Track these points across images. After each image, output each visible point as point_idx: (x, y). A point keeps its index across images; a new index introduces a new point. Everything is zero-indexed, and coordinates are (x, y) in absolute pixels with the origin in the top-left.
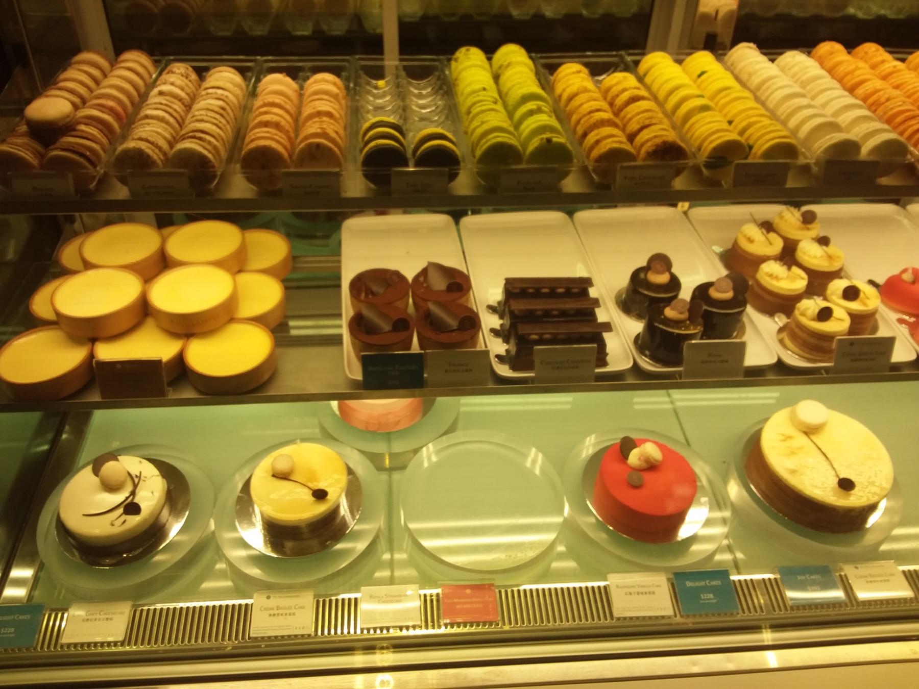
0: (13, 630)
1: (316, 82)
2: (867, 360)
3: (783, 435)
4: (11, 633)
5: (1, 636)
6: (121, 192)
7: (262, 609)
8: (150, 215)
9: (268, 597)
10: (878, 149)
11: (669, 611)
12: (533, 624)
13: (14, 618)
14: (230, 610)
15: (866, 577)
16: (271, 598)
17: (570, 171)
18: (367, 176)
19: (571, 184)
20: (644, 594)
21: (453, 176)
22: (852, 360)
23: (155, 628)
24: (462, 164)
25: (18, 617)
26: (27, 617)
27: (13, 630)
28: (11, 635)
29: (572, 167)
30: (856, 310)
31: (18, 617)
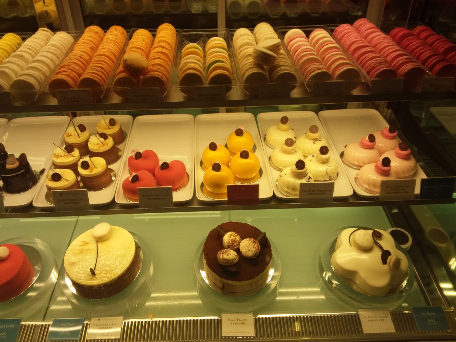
0: (5, 334)
1: (212, 41)
2: (74, 203)
3: (84, 242)
4: (4, 336)
5: (1, 337)
6: (54, 102)
7: (229, 320)
8: (70, 113)
9: (99, 320)
10: (342, 75)
11: (394, 331)
12: (195, 340)
13: (5, 326)
14: (175, 323)
15: (100, 325)
16: (101, 320)
17: (296, 86)
18: (182, 91)
19: (296, 93)
20: (378, 321)
21: (229, 89)
22: (65, 203)
23: (178, 331)
24: (233, 82)
25: (7, 326)
26: (12, 326)
27: (5, 334)
28: (4, 337)
29: (297, 83)
30: (85, 175)
31: (7, 326)
